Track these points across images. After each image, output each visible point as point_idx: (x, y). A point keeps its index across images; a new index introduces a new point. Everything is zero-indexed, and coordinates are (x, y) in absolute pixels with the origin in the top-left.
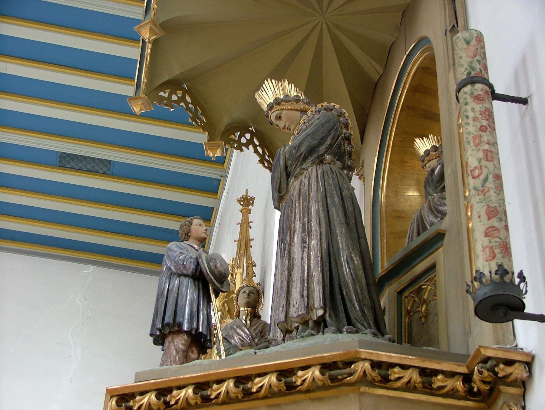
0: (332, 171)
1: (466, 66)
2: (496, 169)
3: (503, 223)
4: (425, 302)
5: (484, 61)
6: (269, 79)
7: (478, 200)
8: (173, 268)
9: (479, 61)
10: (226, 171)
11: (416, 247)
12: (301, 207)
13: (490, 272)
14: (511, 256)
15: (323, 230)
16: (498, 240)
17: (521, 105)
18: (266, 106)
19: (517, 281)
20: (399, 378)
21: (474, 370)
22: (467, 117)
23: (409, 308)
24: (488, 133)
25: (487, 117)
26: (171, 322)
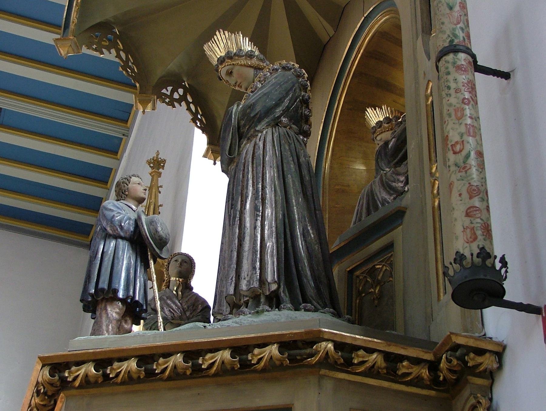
0: (289, 136)
1: (448, 32)
2: (479, 146)
3: (485, 204)
4: (379, 283)
5: (468, 29)
6: (221, 31)
7: (459, 177)
8: (108, 229)
9: (462, 29)
10: (129, 130)
11: (373, 223)
12: (255, 171)
13: (472, 255)
14: (492, 239)
15: (279, 198)
16: (479, 220)
17: (504, 79)
18: (216, 59)
19: (498, 265)
20: (363, 362)
21: (441, 358)
22: (449, 88)
23: (360, 288)
24: (470, 106)
25: (470, 90)
26: (106, 287)
